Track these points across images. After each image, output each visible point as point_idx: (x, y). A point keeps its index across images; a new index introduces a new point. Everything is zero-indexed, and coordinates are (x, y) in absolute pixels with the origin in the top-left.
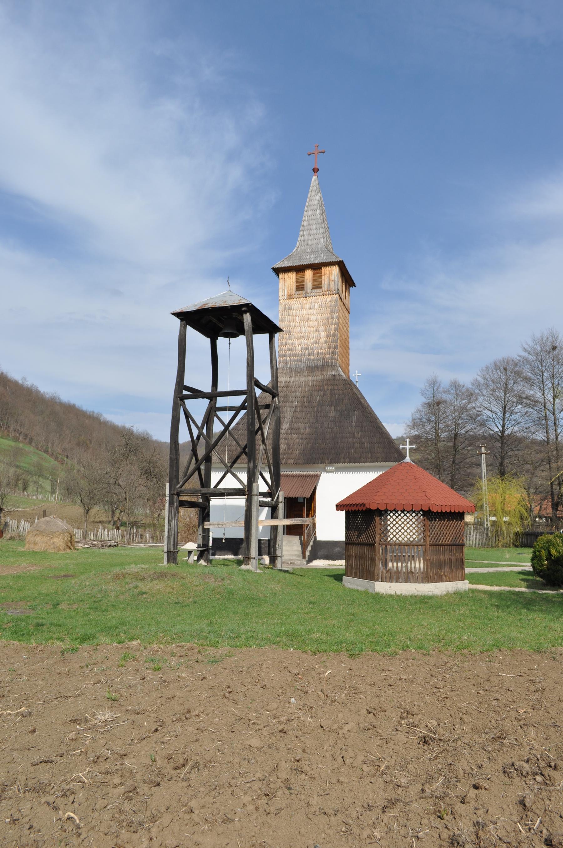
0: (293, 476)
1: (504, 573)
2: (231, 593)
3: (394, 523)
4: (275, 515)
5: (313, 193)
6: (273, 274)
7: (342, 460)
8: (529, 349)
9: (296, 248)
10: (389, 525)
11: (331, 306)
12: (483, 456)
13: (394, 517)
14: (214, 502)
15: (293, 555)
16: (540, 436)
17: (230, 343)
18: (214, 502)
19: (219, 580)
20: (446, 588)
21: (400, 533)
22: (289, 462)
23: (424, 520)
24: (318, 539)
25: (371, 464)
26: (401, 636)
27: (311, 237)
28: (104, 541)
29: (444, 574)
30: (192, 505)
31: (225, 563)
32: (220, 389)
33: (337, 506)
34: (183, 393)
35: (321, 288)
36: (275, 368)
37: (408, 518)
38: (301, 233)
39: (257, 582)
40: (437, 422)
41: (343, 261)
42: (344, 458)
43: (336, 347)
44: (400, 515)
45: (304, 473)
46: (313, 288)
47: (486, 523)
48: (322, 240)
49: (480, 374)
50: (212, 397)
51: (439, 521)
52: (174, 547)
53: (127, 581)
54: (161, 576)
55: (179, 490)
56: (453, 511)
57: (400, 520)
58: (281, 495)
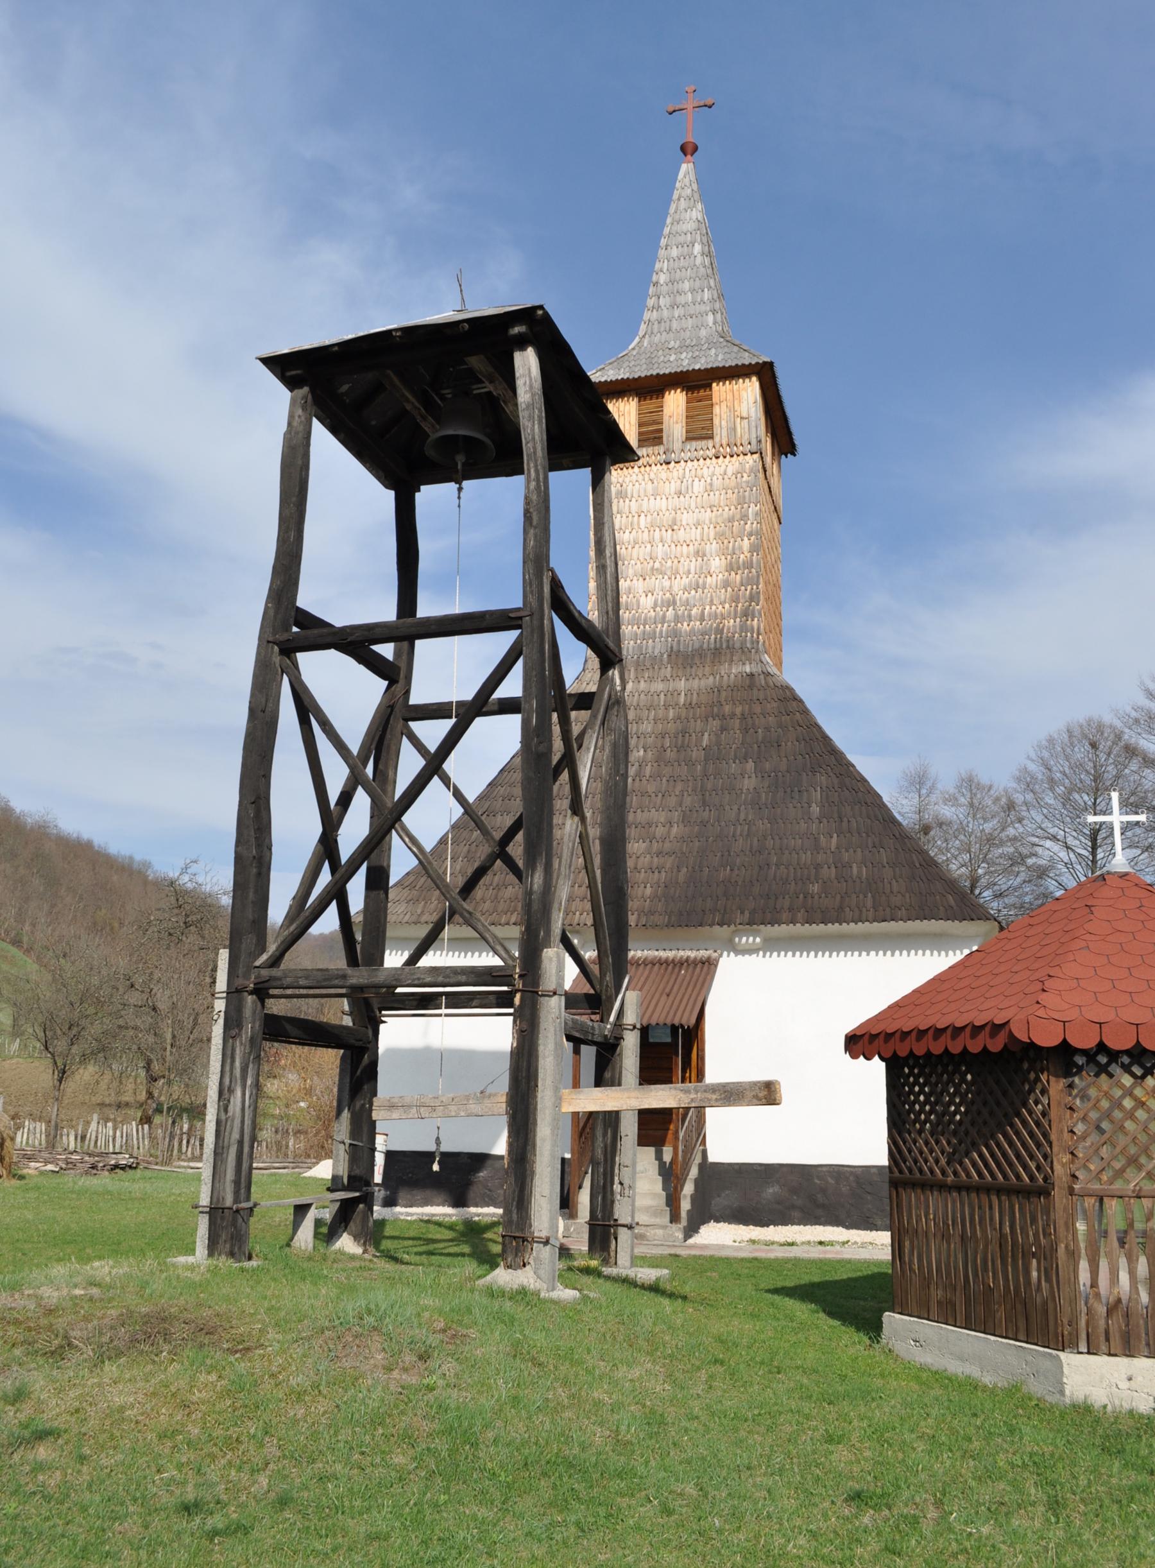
4: (607, 1075)
5: (683, 204)
7: (785, 916)
9: (637, 339)
14: (397, 1033)
18: (397, 1033)
19: (409, 1358)
24: (713, 1158)
25: (862, 927)
28: (100, 1154)
30: (316, 1034)
31: (426, 1242)
32: (427, 608)
34: (291, 632)
35: (711, 437)
36: (610, 570)
38: (651, 302)
41: (771, 364)
42: (790, 910)
43: (753, 598)
45: (670, 954)
46: (688, 439)
52: (237, 1193)
54: (150, 1332)
55: (265, 973)
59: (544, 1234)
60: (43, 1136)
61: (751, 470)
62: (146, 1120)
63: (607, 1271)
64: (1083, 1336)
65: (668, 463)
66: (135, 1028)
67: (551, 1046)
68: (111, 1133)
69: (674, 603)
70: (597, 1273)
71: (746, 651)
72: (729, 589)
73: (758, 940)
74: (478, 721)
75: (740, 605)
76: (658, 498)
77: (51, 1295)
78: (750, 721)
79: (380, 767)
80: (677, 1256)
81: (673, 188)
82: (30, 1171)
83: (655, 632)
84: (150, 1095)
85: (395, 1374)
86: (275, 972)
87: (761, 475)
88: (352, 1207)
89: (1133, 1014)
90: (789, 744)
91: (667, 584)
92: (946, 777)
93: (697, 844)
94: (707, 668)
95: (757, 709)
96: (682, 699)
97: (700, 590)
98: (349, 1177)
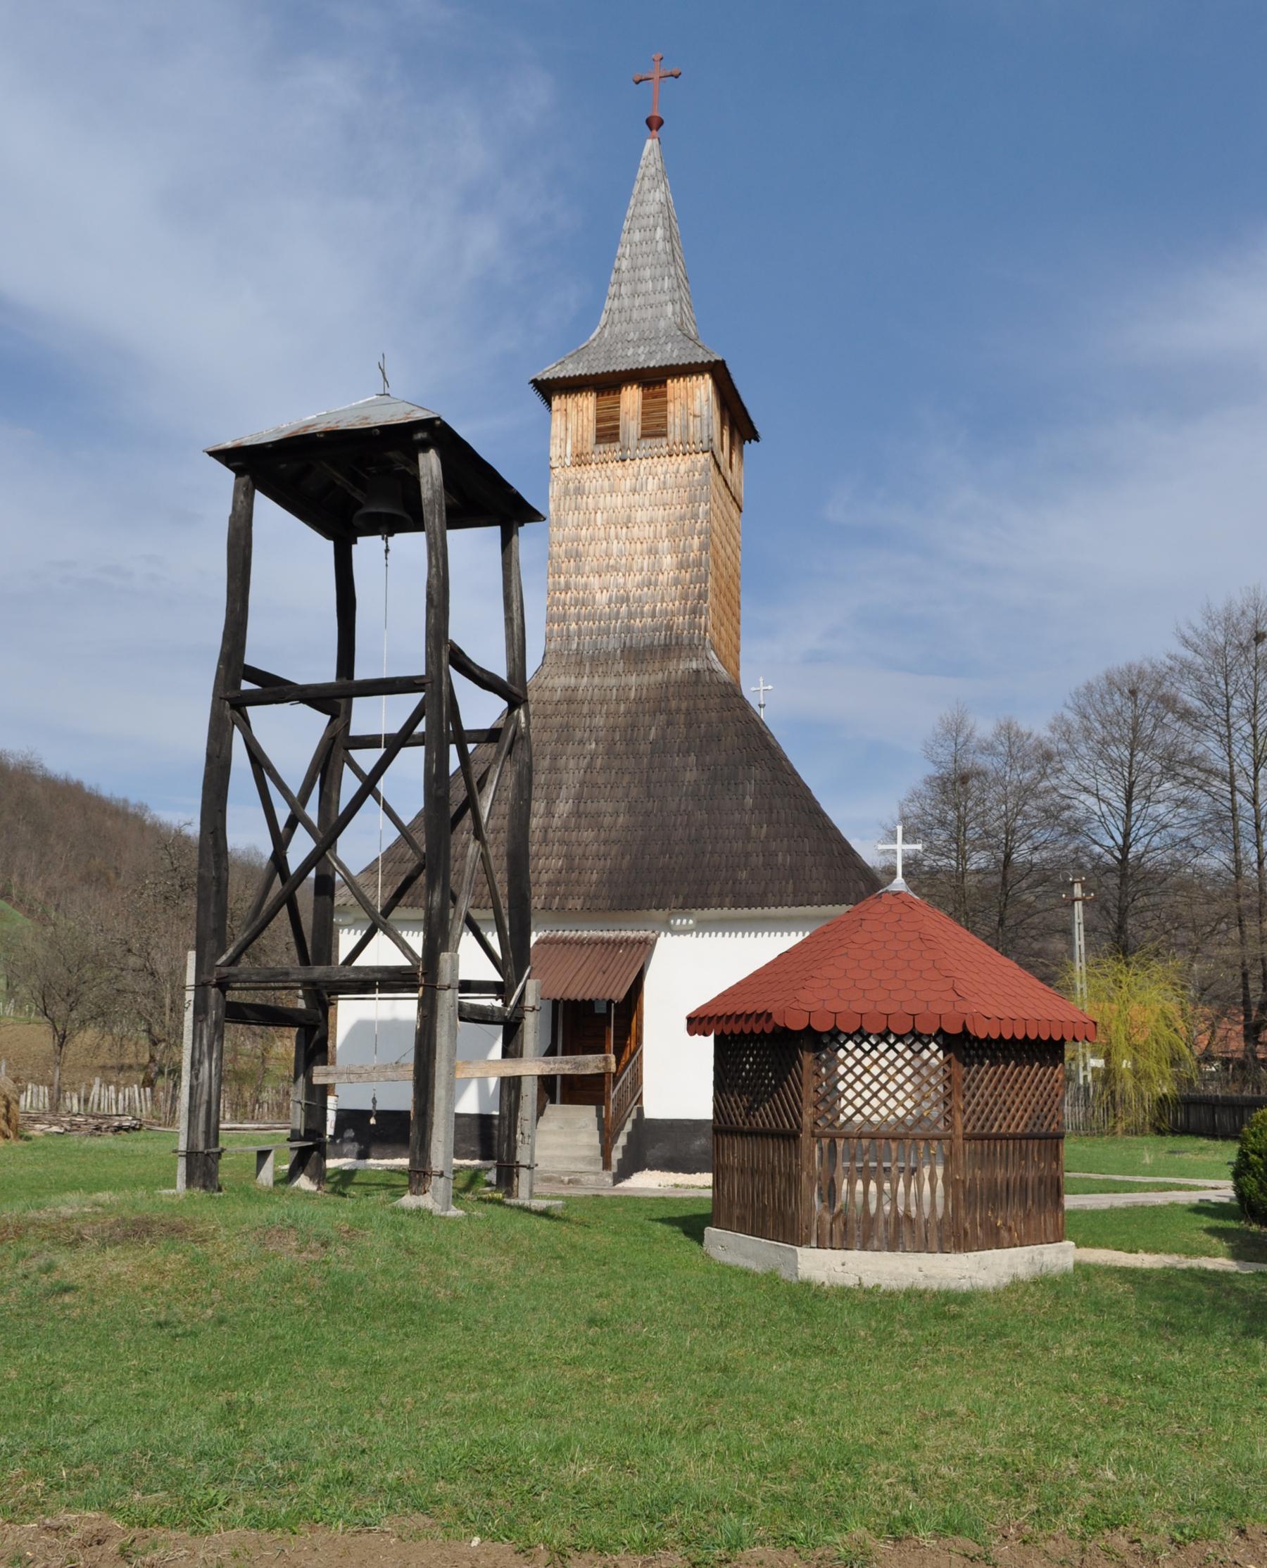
0: (580, 943)
1: (1156, 1210)
2: (342, 1288)
3: (858, 1070)
4: (512, 1048)
6: (535, 398)
7: (714, 900)
8: (1196, 640)
9: (598, 330)
10: (842, 1078)
11: (690, 484)
12: (1078, 906)
13: (859, 1054)
15: (576, 1159)
16: (1217, 860)
17: (387, 551)
19: (314, 1245)
20: (1010, 1266)
21: (875, 1102)
22: (570, 904)
23: (949, 1062)
24: (650, 1113)
26: (883, 1467)
27: (638, 301)
29: (1005, 1224)
30: (274, 1017)
33: (690, 1020)
34: (241, 687)
35: (665, 435)
36: (516, 622)
37: (900, 1055)
38: (612, 290)
39: (438, 1250)
40: (962, 823)
41: (723, 362)
42: (720, 895)
43: (702, 596)
44: (874, 1047)
45: (612, 935)
46: (644, 436)
47: (1081, 1075)
48: (670, 308)
49: (1071, 705)
50: (332, 700)
51: (991, 1065)
52: (207, 1141)
53: (24, 1247)
54: (137, 1231)
55: (225, 970)
56: (1032, 1036)
57: (876, 1062)
58: (532, 990)
59: (439, 1169)
60: (47, 1100)
61: (702, 469)
62: (149, 1083)
63: (508, 1201)
64: (815, 1236)
65: (624, 460)
66: (134, 992)
67: (446, 1028)
68: (113, 1096)
69: (628, 599)
70: (500, 1203)
71: (693, 648)
73: (691, 922)
74: (403, 750)
77: (66, 1211)
79: (326, 790)
80: (598, 1196)
81: (637, 166)
82: (36, 1133)
84: (152, 1058)
85: (304, 1255)
86: (233, 970)
87: (713, 471)
88: (309, 1153)
89: (859, 1007)
91: (621, 581)
92: (984, 728)
93: (640, 833)
94: (657, 664)
98: (306, 1130)
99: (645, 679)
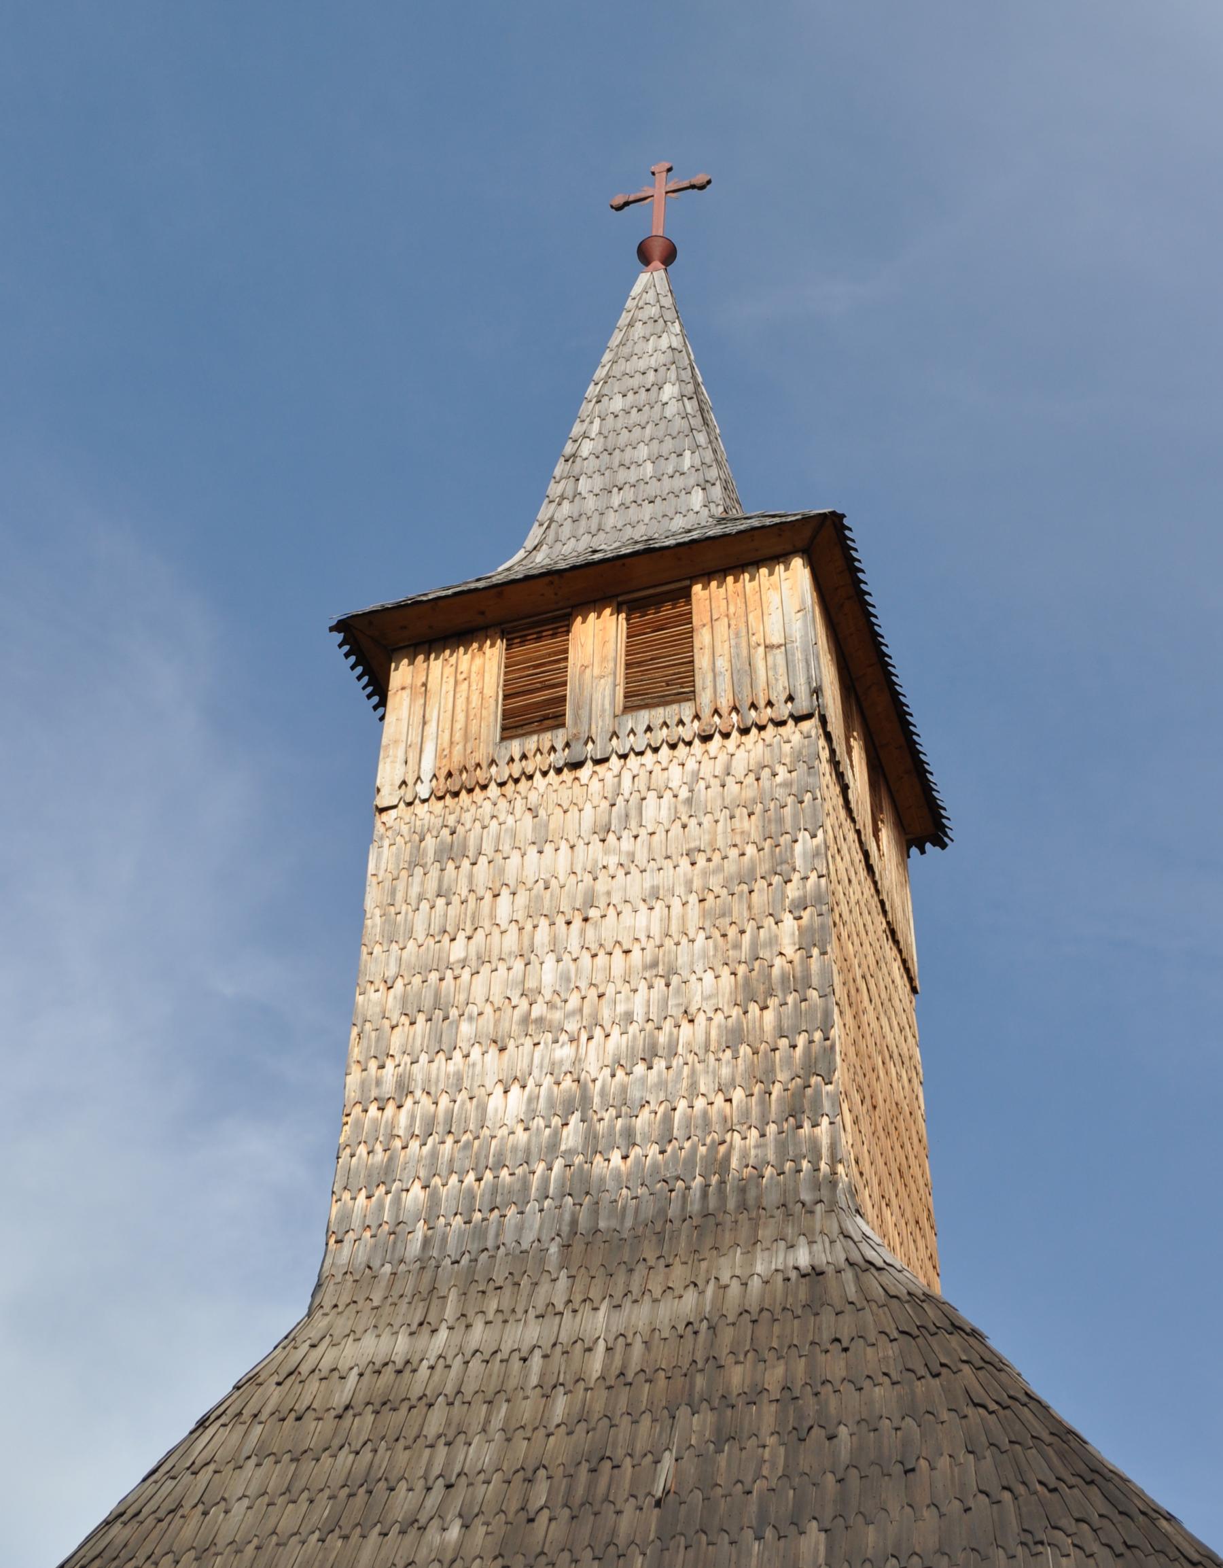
6: (338, 668)
46: (627, 709)
69: (586, 1100)
72: (744, 1050)
75: (776, 1090)
76: (549, 848)
78: (810, 1405)
83: (526, 1186)
90: (943, 1462)
94: (679, 1271)
95: (835, 1366)
96: (596, 1363)
97: (660, 1064)
99: (640, 1316)
